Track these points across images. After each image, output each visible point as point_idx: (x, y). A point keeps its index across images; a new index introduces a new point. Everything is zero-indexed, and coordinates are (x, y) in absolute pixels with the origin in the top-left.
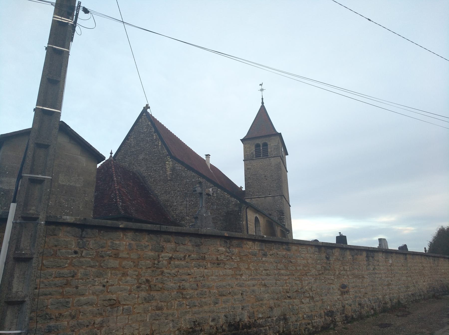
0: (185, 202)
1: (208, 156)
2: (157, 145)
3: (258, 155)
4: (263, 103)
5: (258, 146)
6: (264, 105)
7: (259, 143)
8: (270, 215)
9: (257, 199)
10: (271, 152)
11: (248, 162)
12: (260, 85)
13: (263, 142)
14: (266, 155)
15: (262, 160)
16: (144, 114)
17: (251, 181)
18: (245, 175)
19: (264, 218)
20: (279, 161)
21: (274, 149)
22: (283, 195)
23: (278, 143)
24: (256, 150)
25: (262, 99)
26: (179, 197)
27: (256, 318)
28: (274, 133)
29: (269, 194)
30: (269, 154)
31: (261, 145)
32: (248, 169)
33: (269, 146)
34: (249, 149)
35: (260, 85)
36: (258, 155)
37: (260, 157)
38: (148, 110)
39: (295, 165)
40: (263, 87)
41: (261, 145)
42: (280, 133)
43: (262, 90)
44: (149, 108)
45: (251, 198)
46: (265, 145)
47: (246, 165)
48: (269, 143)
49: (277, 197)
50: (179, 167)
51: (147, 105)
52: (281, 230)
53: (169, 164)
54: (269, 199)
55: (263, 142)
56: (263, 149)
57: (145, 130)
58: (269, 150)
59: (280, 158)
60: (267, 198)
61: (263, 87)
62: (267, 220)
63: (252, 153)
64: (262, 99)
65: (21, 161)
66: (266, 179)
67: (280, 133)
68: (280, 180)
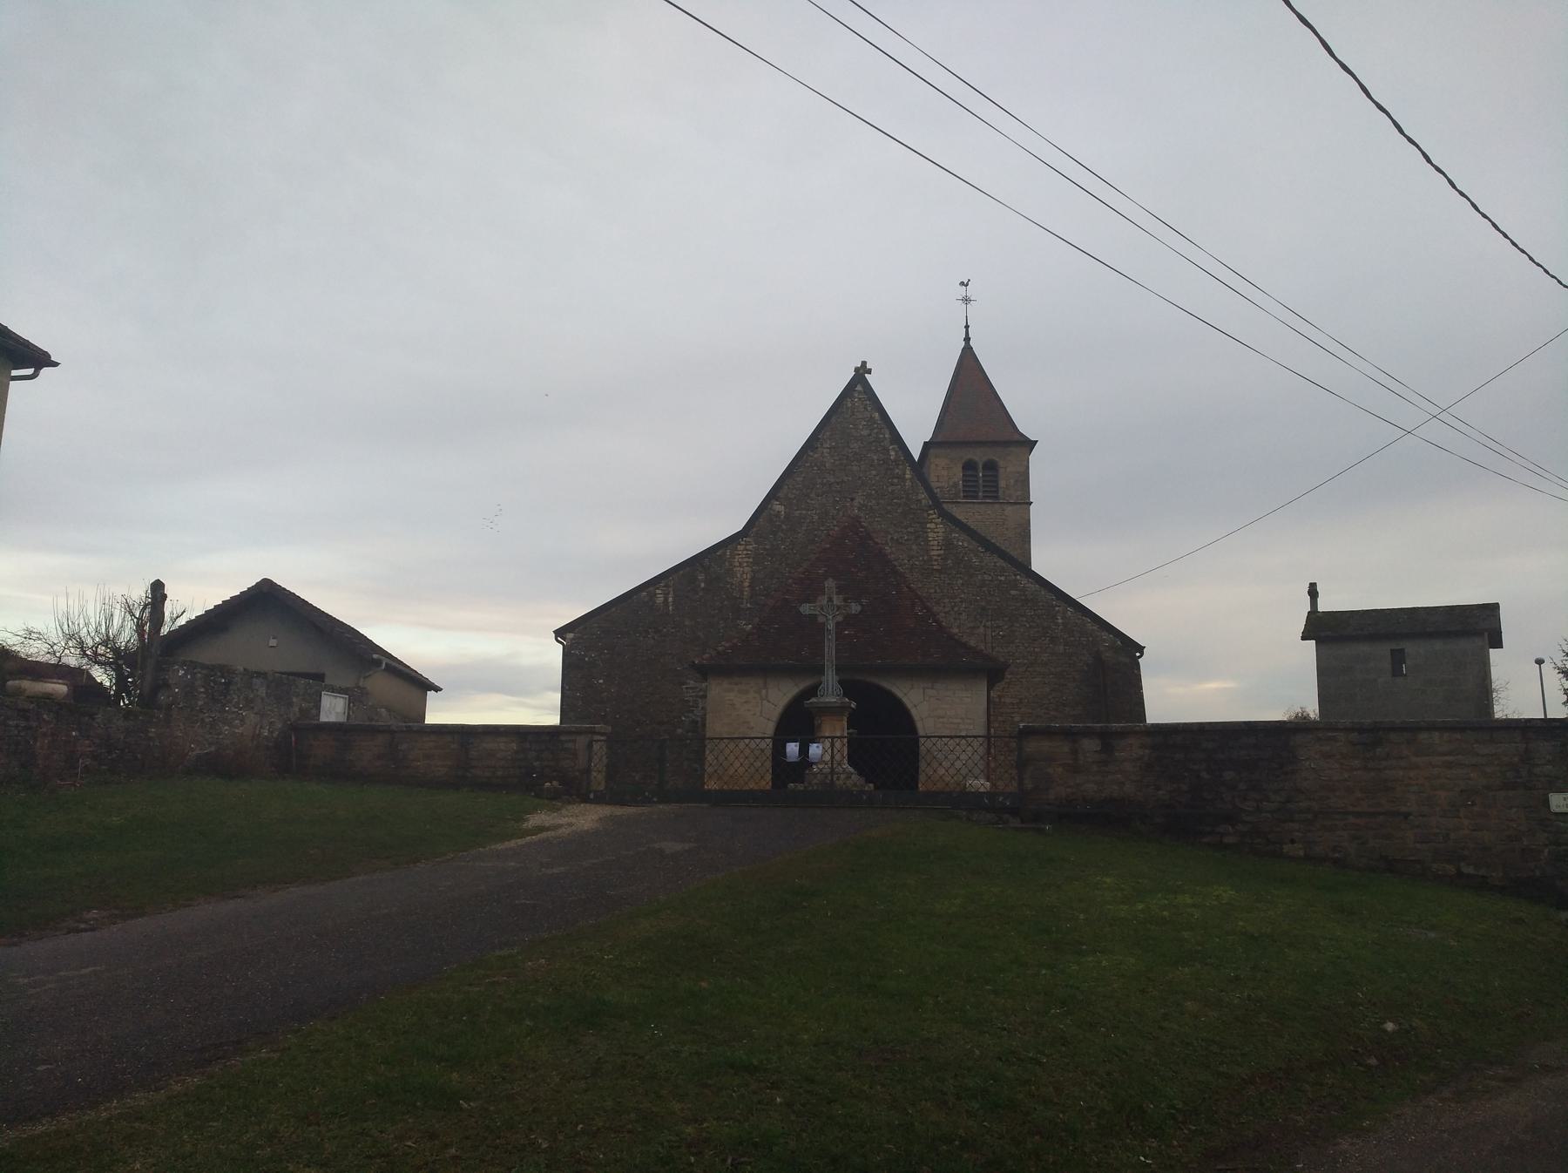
0: (982, 630)
2: (902, 478)
4: (967, 339)
5: (969, 466)
12: (962, 284)
16: (859, 388)
25: (967, 327)
26: (964, 616)
27: (85, 661)
33: (1001, 471)
34: (945, 473)
35: (962, 284)
44: (869, 372)
46: (991, 466)
48: (1001, 463)
50: (961, 541)
51: (864, 363)
53: (936, 530)
57: (865, 433)
58: (1002, 484)
63: (955, 485)
64: (967, 327)
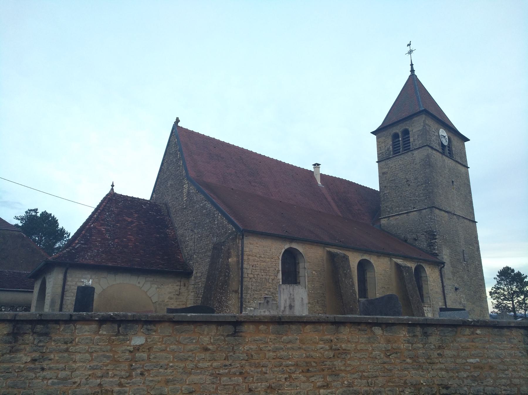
1: (317, 165)
3: (396, 151)
4: (412, 71)
5: (396, 136)
6: (416, 73)
7: (397, 131)
8: (415, 240)
9: (397, 217)
11: (383, 163)
14: (407, 148)
15: (402, 156)
17: (388, 191)
18: (380, 184)
21: (418, 136)
24: (393, 143)
25: (412, 65)
29: (414, 208)
31: (400, 135)
32: (384, 173)
33: (410, 133)
34: (383, 145)
36: (396, 151)
37: (399, 152)
38: (180, 124)
40: (408, 49)
43: (410, 52)
45: (389, 217)
46: (406, 132)
47: (380, 168)
48: (410, 129)
49: (424, 211)
54: (414, 215)
55: (415, 126)
58: (411, 140)
63: (388, 149)
64: (412, 65)
65: (420, 149)
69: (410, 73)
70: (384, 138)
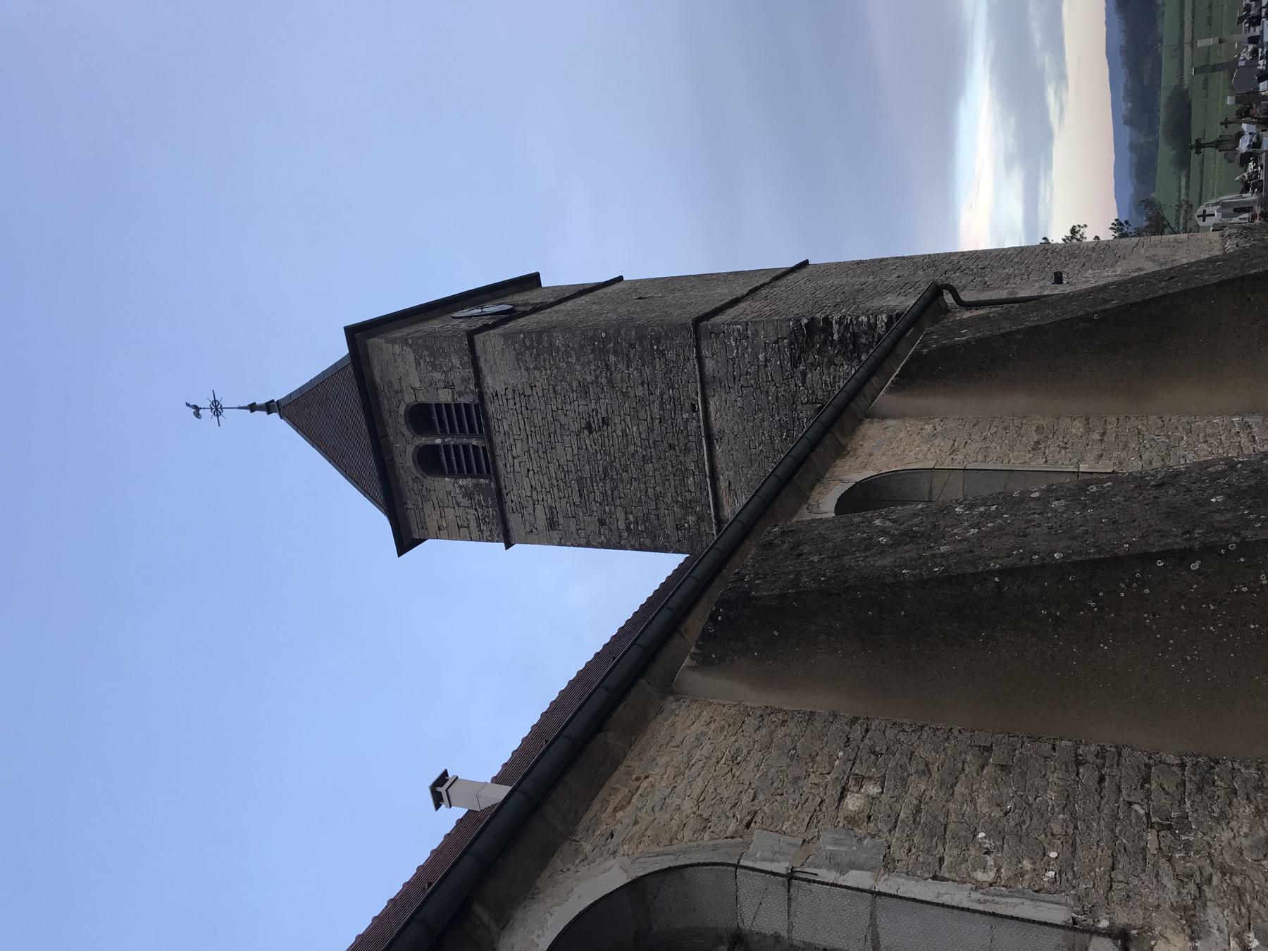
1: (441, 790)
3: (479, 464)
4: (269, 407)
5: (430, 461)
7: (410, 449)
9: (723, 485)
10: (449, 385)
11: (514, 520)
12: (197, 415)
13: (424, 418)
14: (472, 416)
19: (669, 688)
20: (500, 343)
22: (697, 321)
23: (404, 341)
24: (451, 473)
25: (253, 408)
28: (350, 368)
30: (461, 400)
31: (423, 441)
32: (552, 524)
34: (450, 513)
35: (197, 415)
39: (617, 218)
40: (205, 403)
41: (423, 441)
42: (356, 334)
43: (217, 408)
46: (421, 417)
47: (532, 536)
48: (409, 399)
49: (709, 364)
52: (897, 387)
56: (443, 433)
58: (445, 396)
59: (479, 339)
60: (716, 427)
61: (205, 403)
62: (704, 662)
63: (469, 495)
64: (253, 408)
66: (605, 421)
67: (356, 334)
68: (604, 342)
69: (275, 415)
70: (428, 509)
